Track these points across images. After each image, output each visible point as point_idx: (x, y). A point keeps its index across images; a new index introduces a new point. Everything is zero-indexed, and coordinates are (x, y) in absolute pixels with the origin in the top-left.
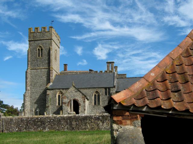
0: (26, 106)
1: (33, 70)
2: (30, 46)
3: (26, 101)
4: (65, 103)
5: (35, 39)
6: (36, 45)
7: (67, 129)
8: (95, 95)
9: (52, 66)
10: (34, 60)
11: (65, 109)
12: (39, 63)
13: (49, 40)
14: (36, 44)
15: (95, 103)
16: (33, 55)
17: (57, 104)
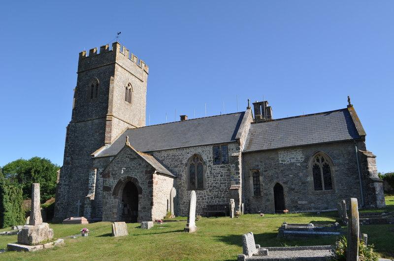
8: (316, 168)
9: (111, 112)
10: (83, 106)
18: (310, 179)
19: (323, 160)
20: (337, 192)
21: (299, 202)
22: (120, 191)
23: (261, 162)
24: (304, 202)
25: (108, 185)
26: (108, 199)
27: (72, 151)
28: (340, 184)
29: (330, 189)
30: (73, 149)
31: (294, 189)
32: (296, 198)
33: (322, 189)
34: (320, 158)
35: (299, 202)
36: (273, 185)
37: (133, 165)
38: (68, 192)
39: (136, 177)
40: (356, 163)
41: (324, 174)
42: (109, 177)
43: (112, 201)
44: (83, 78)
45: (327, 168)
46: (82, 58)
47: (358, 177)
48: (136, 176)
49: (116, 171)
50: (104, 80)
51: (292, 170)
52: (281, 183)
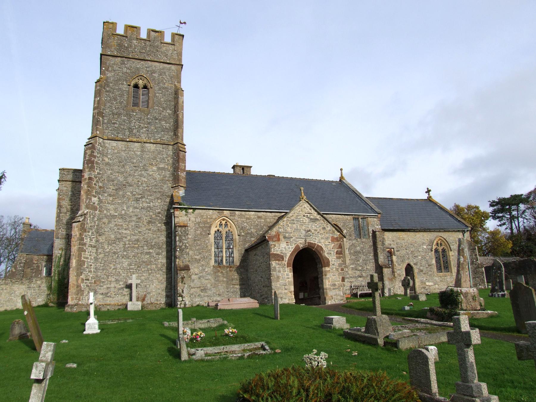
1: (114, 143)
4: (279, 257)
10: (119, 114)
12: (134, 124)
13: (173, 67)
14: (128, 68)
16: (115, 99)
17: (212, 262)
21: (427, 284)
22: (518, 258)
23: (393, 241)
24: (430, 284)
25: (279, 253)
26: (279, 271)
27: (100, 187)
30: (101, 184)
31: (422, 271)
32: (425, 279)
35: (427, 284)
38: (96, 259)
39: (320, 244)
42: (279, 240)
48: (320, 242)
52: (412, 264)
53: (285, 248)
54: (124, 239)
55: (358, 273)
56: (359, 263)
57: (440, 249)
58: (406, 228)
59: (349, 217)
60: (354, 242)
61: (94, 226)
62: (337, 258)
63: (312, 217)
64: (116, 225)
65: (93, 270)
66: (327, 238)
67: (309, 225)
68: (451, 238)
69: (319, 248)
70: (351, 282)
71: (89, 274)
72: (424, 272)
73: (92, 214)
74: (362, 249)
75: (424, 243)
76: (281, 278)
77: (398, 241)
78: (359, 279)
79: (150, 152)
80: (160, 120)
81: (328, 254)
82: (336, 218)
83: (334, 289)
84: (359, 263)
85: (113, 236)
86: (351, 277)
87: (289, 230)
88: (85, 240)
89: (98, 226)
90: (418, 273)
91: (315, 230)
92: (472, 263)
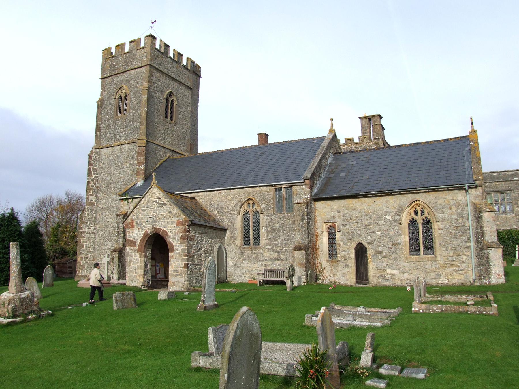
0: (83, 245)
1: (105, 150)
2: (104, 91)
3: (84, 232)
5: (114, 73)
6: (116, 86)
7: (366, 225)
8: (413, 223)
10: (109, 125)
11: (130, 262)
12: (118, 130)
14: (115, 84)
15: (246, 241)
16: (108, 113)
18: (405, 239)
19: (423, 212)
20: (439, 259)
21: (388, 271)
23: (339, 212)
24: (394, 271)
25: (132, 239)
26: (132, 256)
27: (97, 187)
28: (444, 249)
29: (431, 255)
30: (97, 185)
31: (380, 253)
32: (384, 265)
33: (419, 255)
34: (419, 209)
35: (388, 271)
36: (354, 245)
37: (162, 213)
38: (94, 242)
39: (165, 229)
40: (468, 219)
41: (424, 233)
43: (137, 260)
44: (108, 86)
45: (427, 222)
46: (107, 54)
47: (469, 239)
49: (142, 219)
50: (135, 89)
51: (379, 225)
52: (365, 243)
53: (137, 235)
54: (110, 226)
55: (275, 255)
56: (277, 243)
57: (420, 219)
58: (396, 187)
59: (268, 189)
60: (272, 218)
61: (92, 218)
62: (182, 243)
63: (160, 202)
64: (106, 216)
65: (91, 251)
66: (173, 223)
67: (157, 210)
68: (439, 202)
69: (164, 233)
70: (265, 266)
71: (88, 253)
72: (384, 254)
73: (90, 209)
74: (282, 226)
75: (388, 212)
76: (132, 263)
77: (346, 211)
78: (276, 262)
79: (125, 152)
80: (133, 121)
81: (172, 239)
82: (253, 192)
83: (176, 275)
84: (277, 243)
85: (103, 225)
86: (266, 260)
87: (141, 217)
88: (83, 229)
89: (95, 217)
90: (373, 256)
91: (162, 215)
92: (477, 241)
